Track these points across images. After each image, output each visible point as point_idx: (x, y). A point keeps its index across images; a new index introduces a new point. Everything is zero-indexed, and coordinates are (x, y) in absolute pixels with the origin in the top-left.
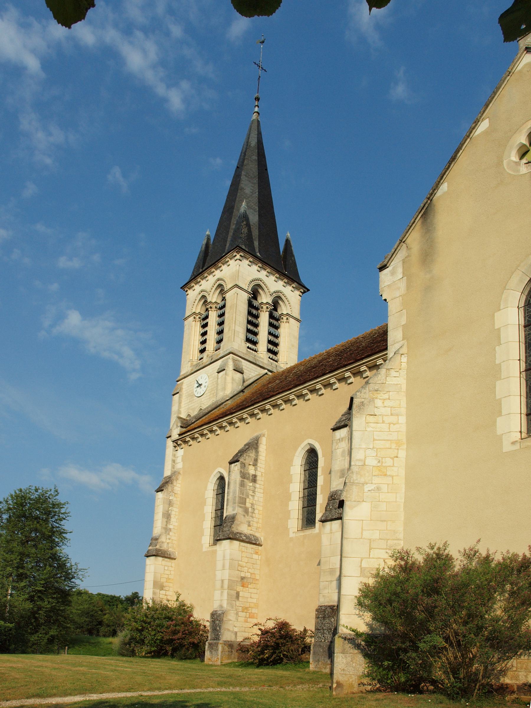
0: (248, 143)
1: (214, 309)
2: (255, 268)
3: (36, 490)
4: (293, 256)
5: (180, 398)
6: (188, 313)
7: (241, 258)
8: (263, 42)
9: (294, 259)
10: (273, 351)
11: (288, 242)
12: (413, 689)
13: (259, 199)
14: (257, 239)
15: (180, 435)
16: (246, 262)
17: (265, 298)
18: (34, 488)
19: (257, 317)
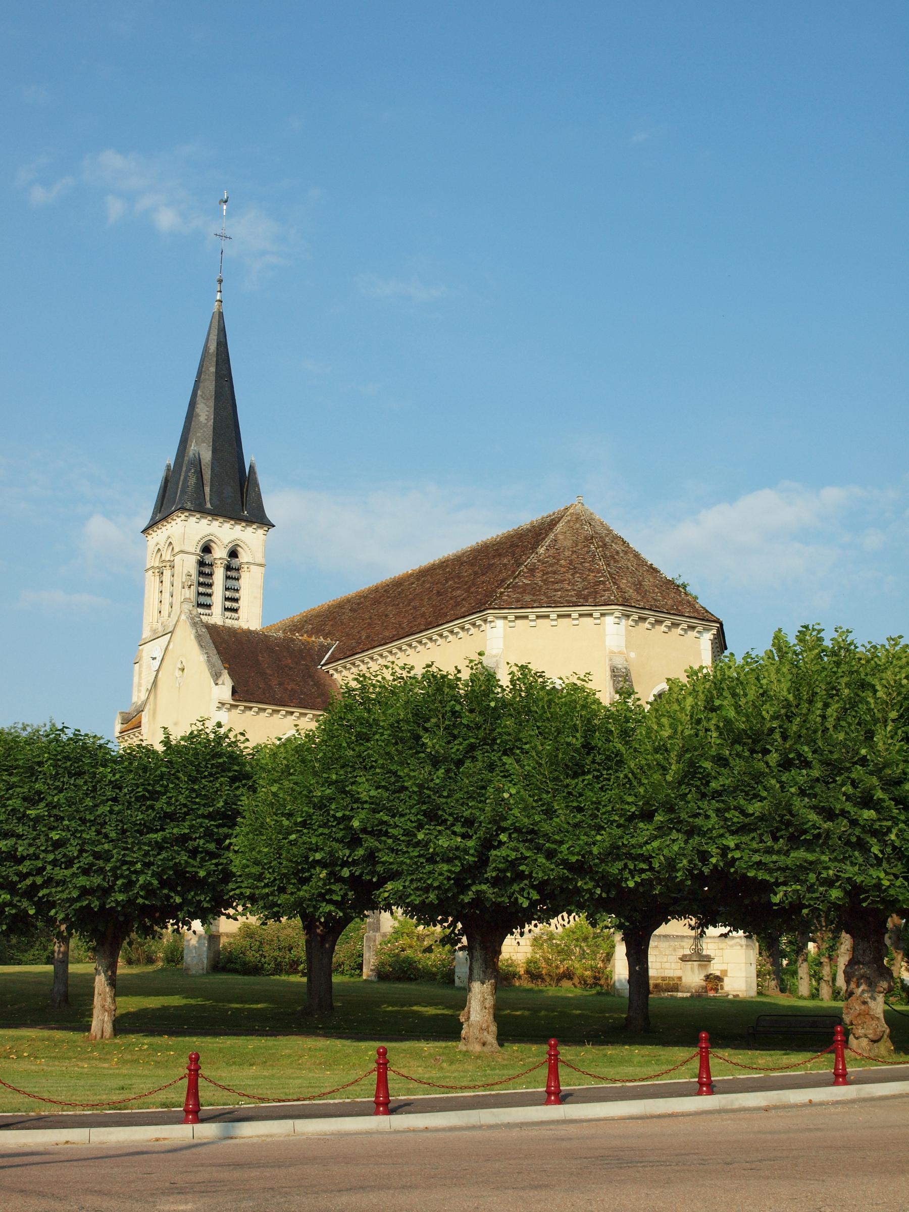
0: (206, 348)
1: (168, 568)
2: (204, 522)
3: (24, 729)
4: (258, 485)
5: (140, 667)
6: (148, 566)
7: (186, 519)
8: (226, 201)
9: (259, 489)
10: (232, 604)
11: (252, 468)
12: (75, 921)
13: (214, 428)
14: (209, 484)
15: (120, 733)
16: (193, 520)
17: (220, 553)
18: (20, 726)
19: (210, 575)
